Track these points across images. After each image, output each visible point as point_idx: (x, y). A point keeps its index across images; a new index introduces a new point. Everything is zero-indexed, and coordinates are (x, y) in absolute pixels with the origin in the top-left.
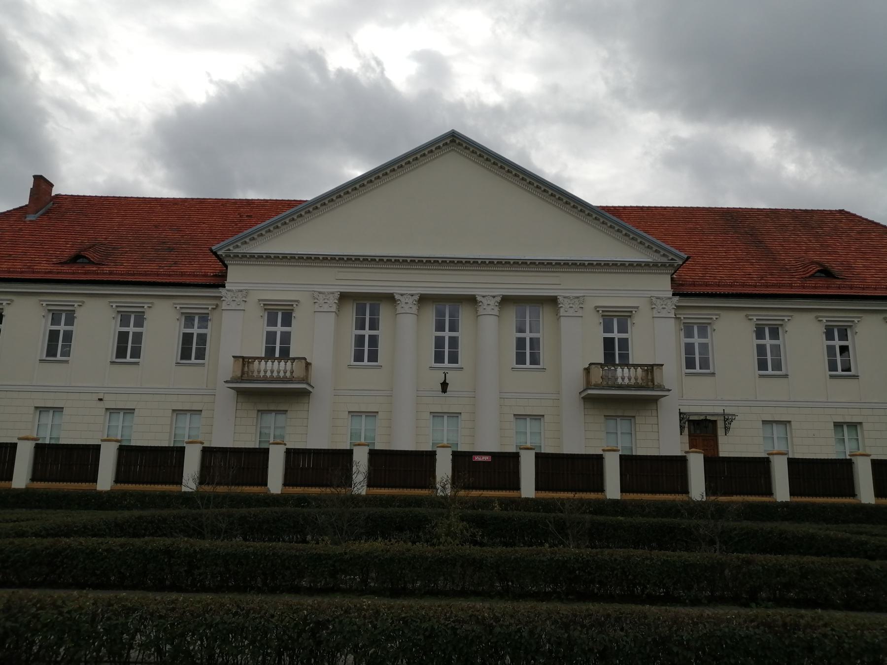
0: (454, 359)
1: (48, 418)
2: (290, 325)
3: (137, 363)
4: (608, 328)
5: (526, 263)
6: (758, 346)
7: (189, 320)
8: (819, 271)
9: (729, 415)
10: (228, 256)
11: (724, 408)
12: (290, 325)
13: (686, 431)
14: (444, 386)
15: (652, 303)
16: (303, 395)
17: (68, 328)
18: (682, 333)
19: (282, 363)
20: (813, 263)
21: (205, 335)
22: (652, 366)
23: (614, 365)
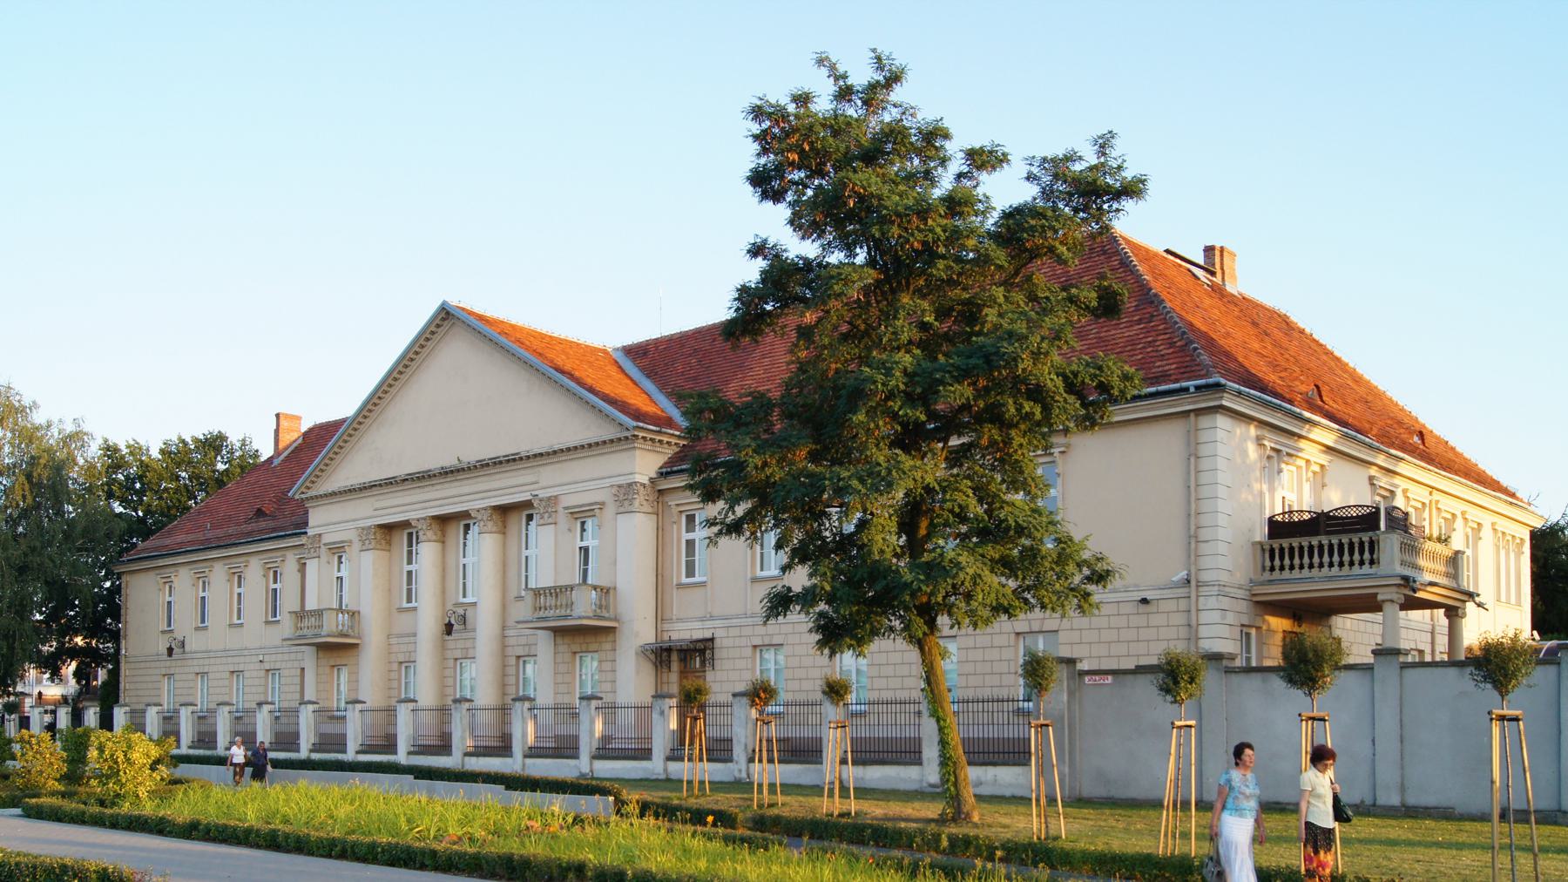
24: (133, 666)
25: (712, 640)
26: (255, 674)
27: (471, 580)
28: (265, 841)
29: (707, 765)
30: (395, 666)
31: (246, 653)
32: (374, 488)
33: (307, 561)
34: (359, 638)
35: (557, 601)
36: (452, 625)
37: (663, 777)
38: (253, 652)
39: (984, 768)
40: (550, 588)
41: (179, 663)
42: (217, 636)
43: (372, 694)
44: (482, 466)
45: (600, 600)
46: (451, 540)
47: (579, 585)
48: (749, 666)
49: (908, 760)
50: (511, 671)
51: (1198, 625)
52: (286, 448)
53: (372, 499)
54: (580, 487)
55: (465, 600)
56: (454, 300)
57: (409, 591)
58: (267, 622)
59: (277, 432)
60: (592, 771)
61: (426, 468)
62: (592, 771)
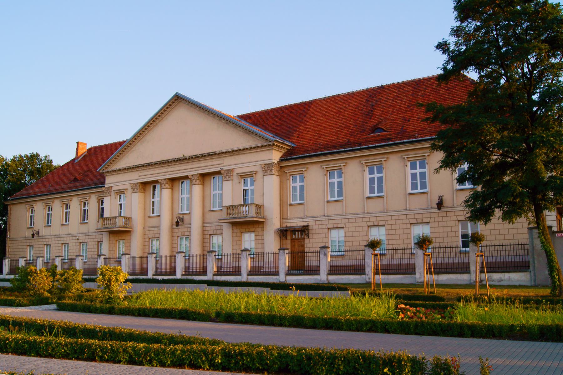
11: (308, 222)
17: (372, 176)
21: (425, 173)
24: (13, 242)
25: (308, 226)
26: (93, 243)
27: (156, 207)
28: (288, 321)
29: (382, 277)
30: (147, 240)
31: (70, 236)
32: (140, 168)
33: (105, 198)
34: (131, 228)
35: (110, 222)
36: (179, 222)
37: (327, 282)
38: (74, 235)
39: (503, 274)
40: (108, 218)
41: (36, 241)
42: (56, 227)
43: (136, 250)
44: (196, 157)
45: (126, 222)
46: (175, 188)
47: (118, 217)
48: (148, 244)
49: (460, 271)
50: (206, 240)
51: (546, 216)
52: (81, 156)
53: (138, 172)
54: (245, 165)
55: (182, 212)
56: (180, 92)
57: (66, 219)
58: (81, 223)
59: (77, 149)
60: (286, 281)
61: (166, 159)
62: (286, 281)
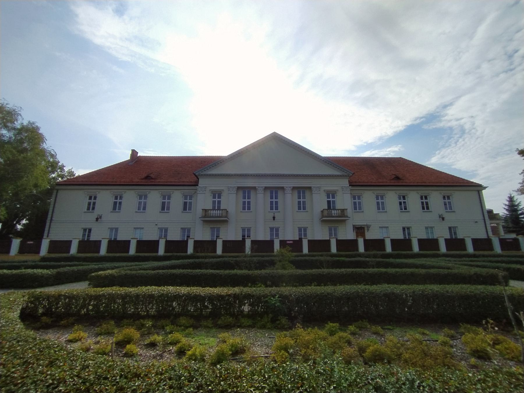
0: (277, 208)
1: (138, 231)
2: (220, 198)
3: (145, 212)
4: (328, 197)
5: (284, 176)
6: (298, 201)
7: (186, 197)
8: (395, 178)
9: (369, 225)
10: (199, 175)
12: (220, 198)
13: (355, 231)
14: (274, 218)
15: (342, 189)
16: (226, 221)
17: (120, 201)
18: (352, 198)
19: (219, 211)
20: (393, 175)
22: (344, 209)
23: (331, 209)
